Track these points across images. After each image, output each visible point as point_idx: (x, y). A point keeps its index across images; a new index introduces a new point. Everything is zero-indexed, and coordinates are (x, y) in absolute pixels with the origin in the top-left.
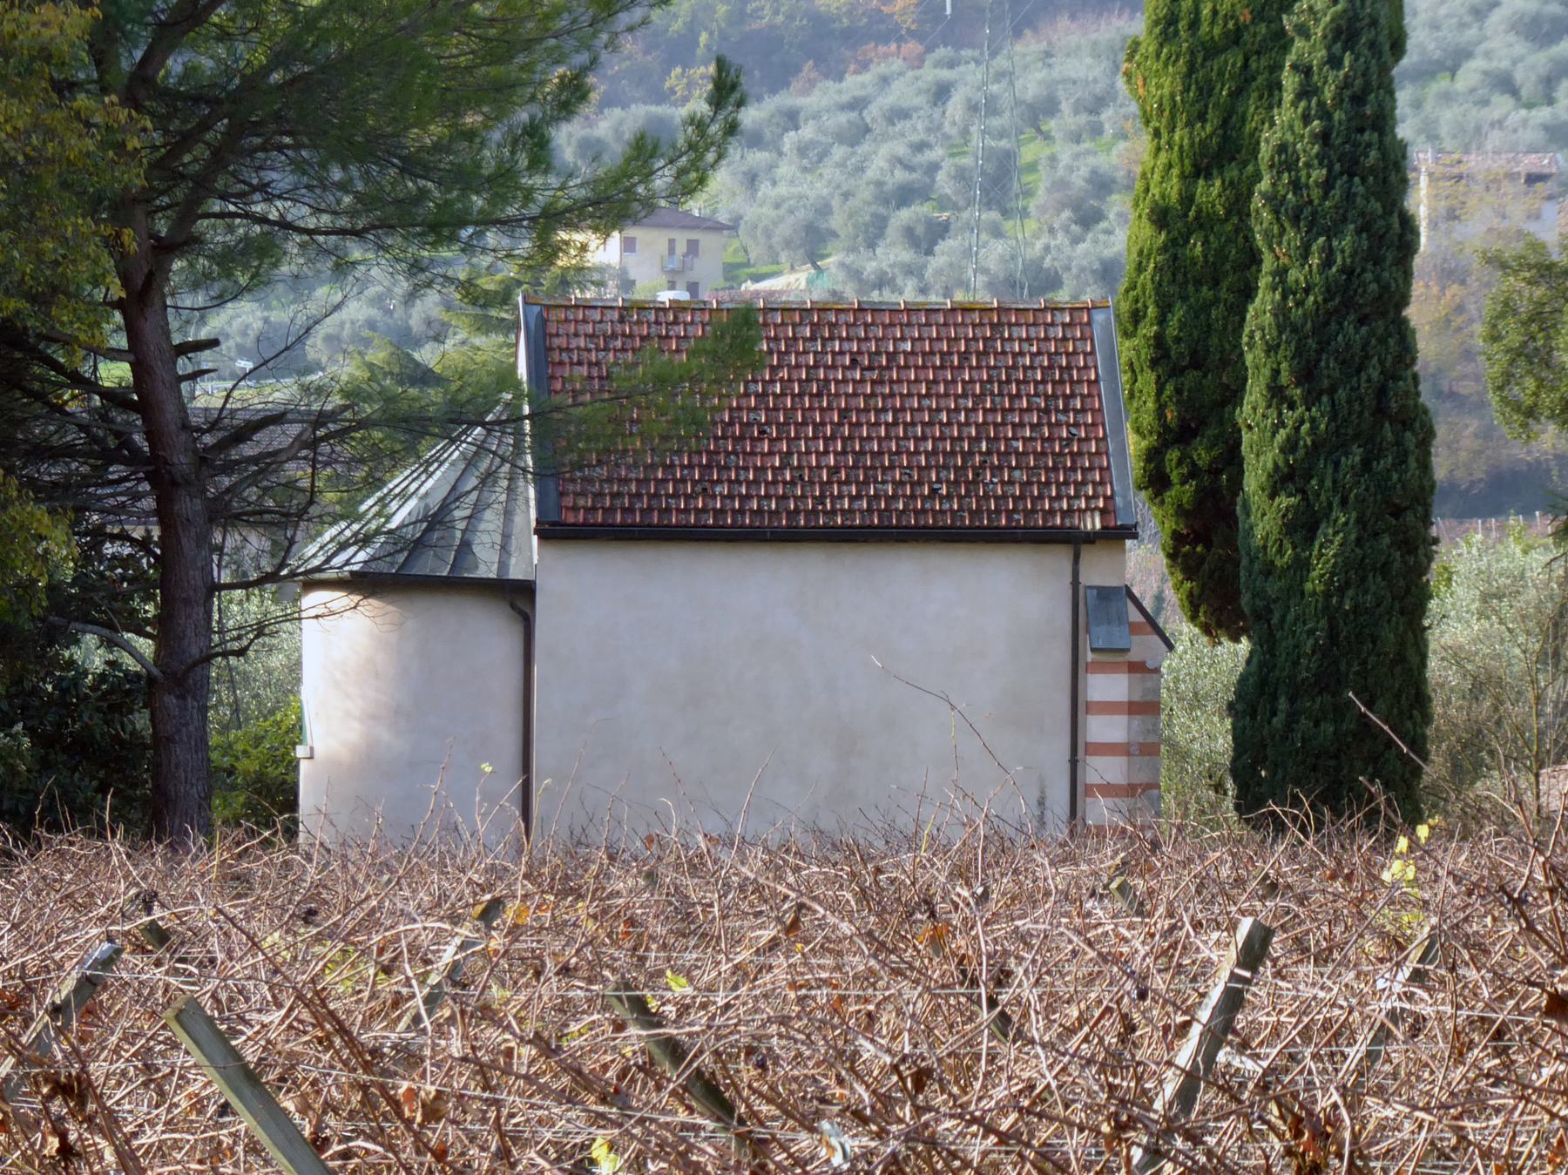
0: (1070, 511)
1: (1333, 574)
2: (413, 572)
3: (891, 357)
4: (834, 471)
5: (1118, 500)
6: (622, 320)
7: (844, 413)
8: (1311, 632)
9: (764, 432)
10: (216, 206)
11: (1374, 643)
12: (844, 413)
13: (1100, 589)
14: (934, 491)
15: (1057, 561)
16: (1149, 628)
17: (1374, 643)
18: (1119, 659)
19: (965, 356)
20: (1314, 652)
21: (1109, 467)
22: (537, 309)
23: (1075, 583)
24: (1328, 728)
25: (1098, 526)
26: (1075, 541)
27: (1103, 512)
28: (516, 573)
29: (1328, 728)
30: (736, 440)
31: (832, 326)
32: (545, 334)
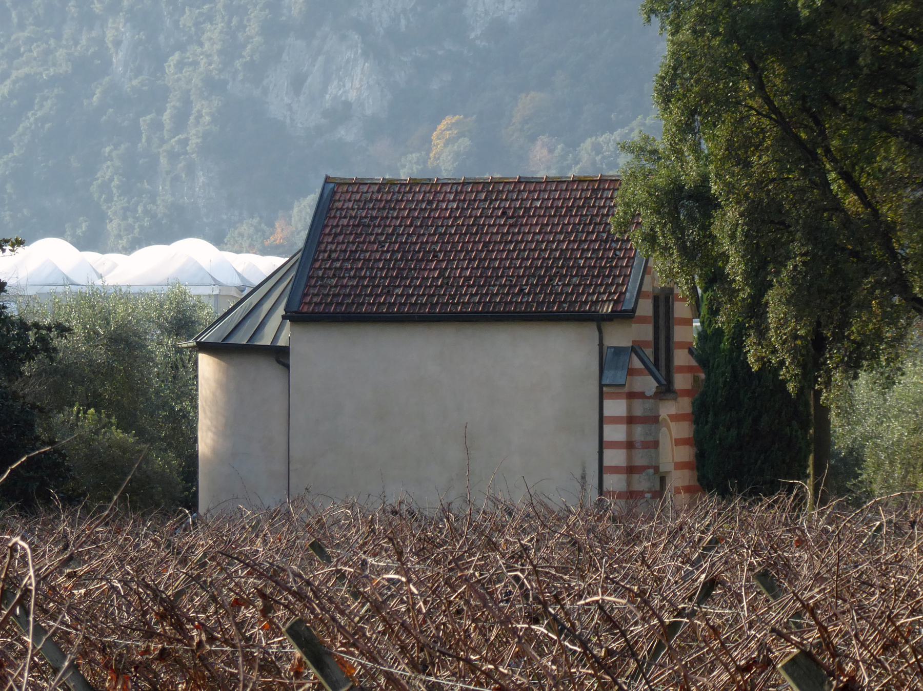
0: (597, 301)
1: (733, 339)
2: (230, 342)
3: (527, 210)
4: (467, 279)
5: (628, 294)
6: (379, 191)
7: (486, 244)
8: (723, 374)
9: (437, 256)
10: (857, 174)
11: (760, 381)
12: (486, 244)
13: (615, 348)
14: (521, 290)
15: (589, 332)
16: (646, 372)
17: (760, 381)
18: (620, 391)
19: (569, 209)
20: (725, 386)
21: (630, 275)
22: (332, 185)
23: (601, 345)
24: (734, 432)
25: (610, 310)
26: (600, 320)
27: (616, 302)
28: (282, 342)
29: (734, 432)
30: (418, 261)
31: (499, 192)
32: (331, 200)
